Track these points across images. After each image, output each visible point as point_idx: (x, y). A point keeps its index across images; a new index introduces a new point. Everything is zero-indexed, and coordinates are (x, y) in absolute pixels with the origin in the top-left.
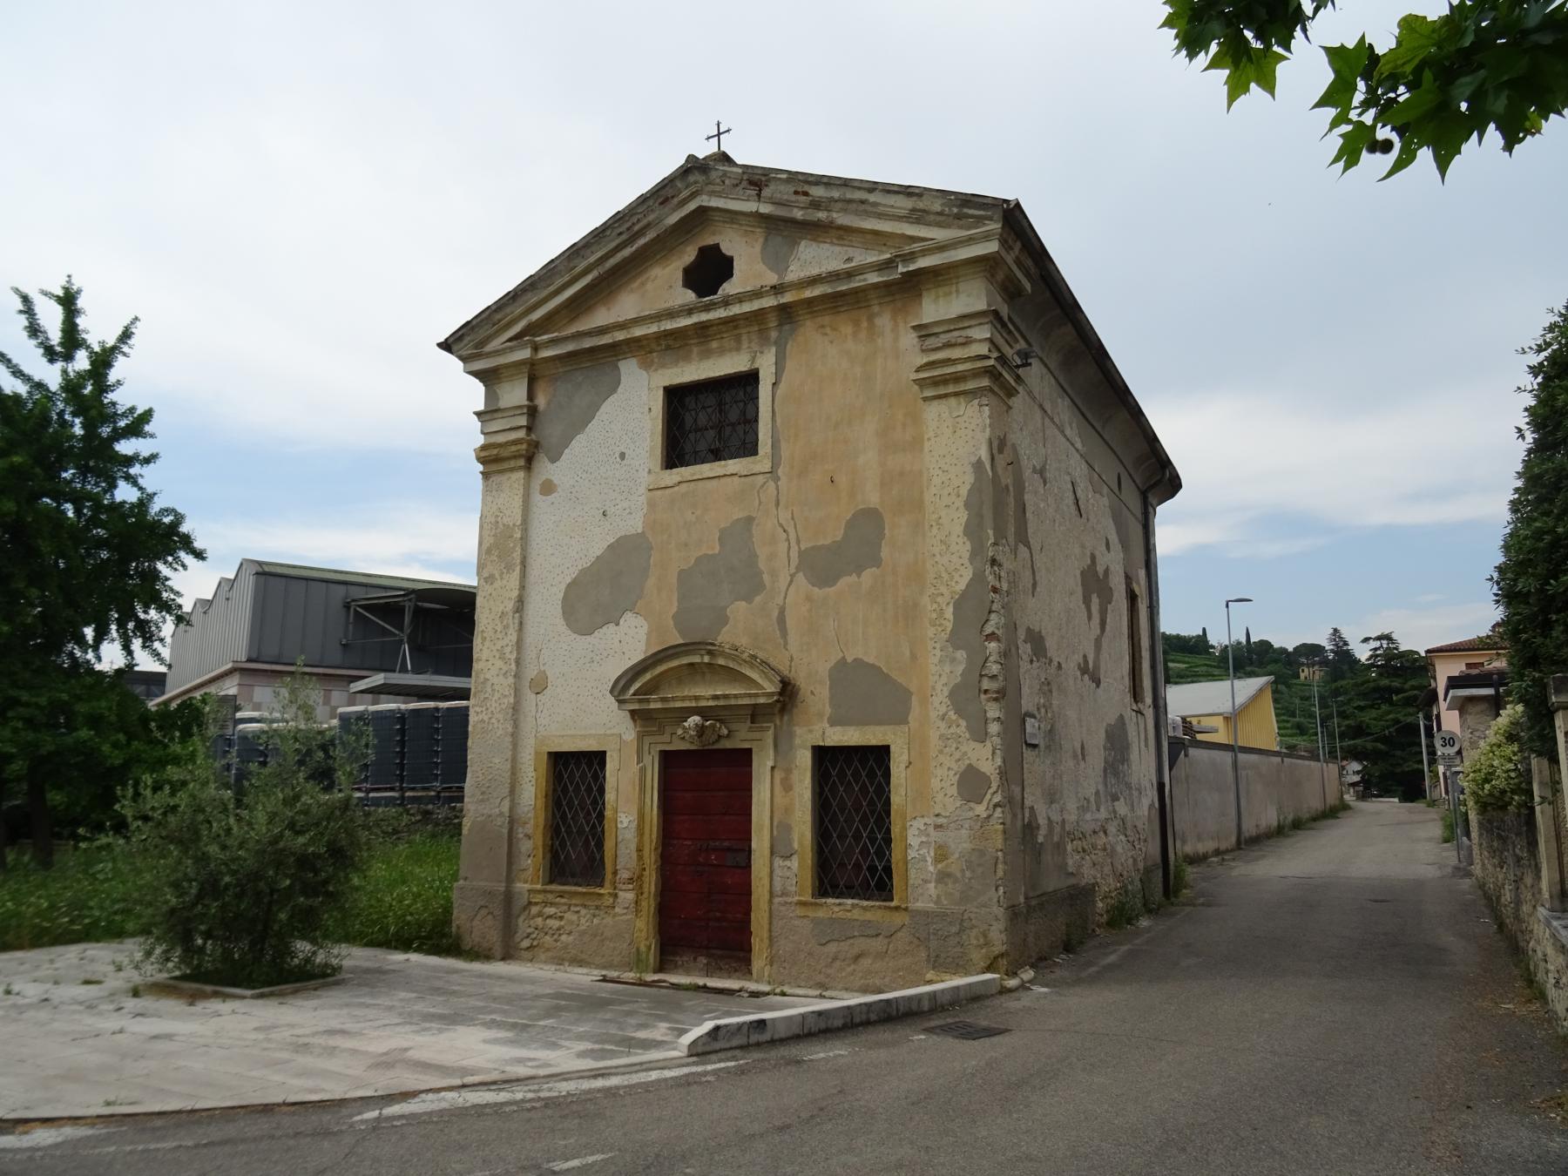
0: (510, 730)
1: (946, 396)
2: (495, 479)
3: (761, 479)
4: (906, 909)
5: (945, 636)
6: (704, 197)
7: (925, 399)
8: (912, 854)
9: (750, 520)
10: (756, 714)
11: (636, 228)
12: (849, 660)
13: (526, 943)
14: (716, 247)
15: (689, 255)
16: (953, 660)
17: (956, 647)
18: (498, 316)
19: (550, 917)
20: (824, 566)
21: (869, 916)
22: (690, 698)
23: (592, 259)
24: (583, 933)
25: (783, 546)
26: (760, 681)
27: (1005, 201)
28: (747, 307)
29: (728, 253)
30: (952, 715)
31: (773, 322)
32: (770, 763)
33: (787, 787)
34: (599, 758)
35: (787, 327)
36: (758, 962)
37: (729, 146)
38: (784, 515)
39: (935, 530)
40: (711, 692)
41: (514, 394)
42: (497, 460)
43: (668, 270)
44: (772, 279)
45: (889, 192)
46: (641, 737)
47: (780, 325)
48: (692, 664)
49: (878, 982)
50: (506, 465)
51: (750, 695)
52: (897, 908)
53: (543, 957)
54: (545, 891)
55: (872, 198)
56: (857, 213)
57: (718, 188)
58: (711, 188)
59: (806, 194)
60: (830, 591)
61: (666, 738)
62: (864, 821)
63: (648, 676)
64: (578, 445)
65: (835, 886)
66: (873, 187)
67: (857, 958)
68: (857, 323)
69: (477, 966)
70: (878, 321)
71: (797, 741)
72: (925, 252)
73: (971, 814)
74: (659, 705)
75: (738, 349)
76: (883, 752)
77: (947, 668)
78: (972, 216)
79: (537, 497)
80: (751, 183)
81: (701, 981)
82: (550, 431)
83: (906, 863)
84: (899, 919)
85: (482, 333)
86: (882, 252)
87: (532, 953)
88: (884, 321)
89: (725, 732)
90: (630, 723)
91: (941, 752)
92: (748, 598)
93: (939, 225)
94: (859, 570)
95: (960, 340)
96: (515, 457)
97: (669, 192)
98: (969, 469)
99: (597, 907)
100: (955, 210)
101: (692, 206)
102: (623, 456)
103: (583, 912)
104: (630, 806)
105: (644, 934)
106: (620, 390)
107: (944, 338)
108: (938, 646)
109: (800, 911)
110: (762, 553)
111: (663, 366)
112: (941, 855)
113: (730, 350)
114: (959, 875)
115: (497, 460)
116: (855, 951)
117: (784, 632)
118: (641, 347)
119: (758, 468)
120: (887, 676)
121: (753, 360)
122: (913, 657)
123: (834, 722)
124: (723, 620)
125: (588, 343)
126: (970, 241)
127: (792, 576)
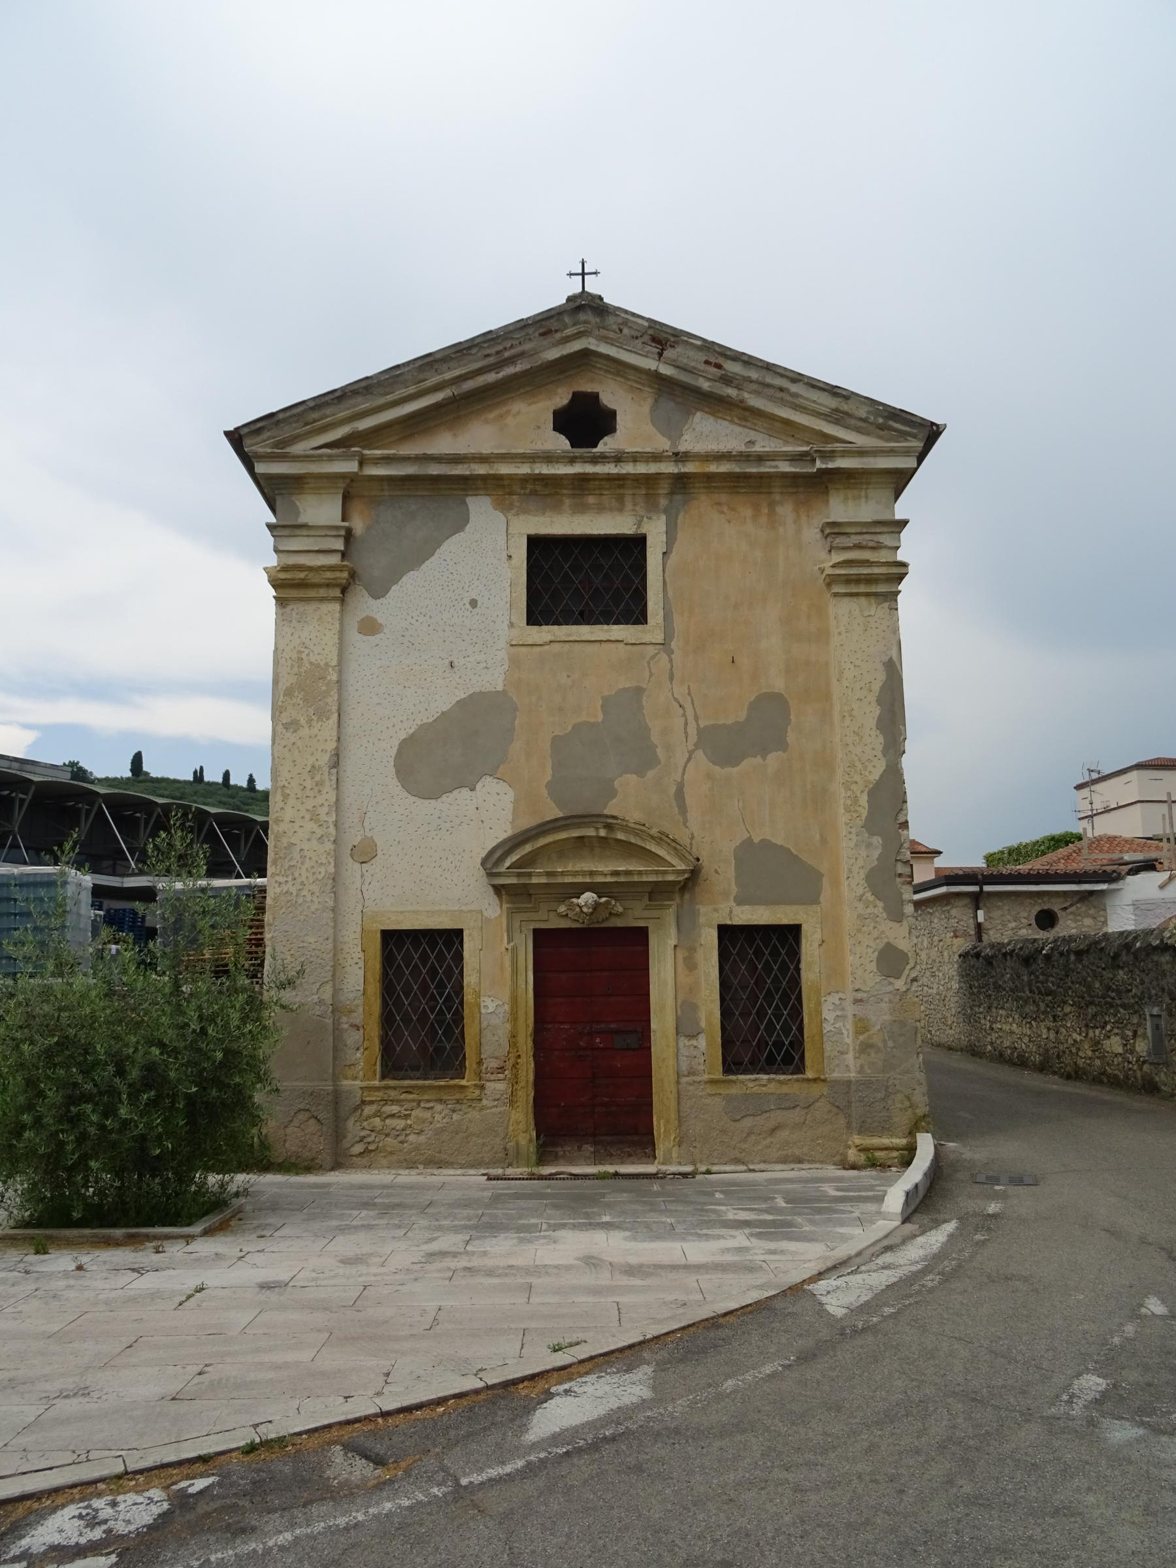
0: (331, 903)
1: (857, 595)
2: (295, 609)
3: (651, 650)
4: (824, 1081)
5: (861, 823)
6: (591, 340)
7: (836, 595)
8: (827, 1027)
9: (639, 691)
10: (658, 892)
11: (507, 354)
12: (756, 840)
13: (358, 1148)
14: (595, 397)
15: (561, 398)
16: (869, 845)
17: (872, 834)
18: (315, 415)
19: (393, 1116)
20: (724, 746)
21: (785, 1089)
22: (583, 873)
23: (448, 376)
24: (439, 1132)
25: (678, 722)
26: (668, 858)
27: (933, 424)
28: (641, 469)
29: (612, 406)
30: (869, 896)
31: (664, 488)
32: (673, 942)
33: (691, 965)
34: (454, 937)
35: (678, 497)
36: (664, 1142)
37: (593, 286)
38: (680, 691)
39: (847, 721)
40: (611, 868)
41: (322, 510)
42: (302, 585)
43: (533, 407)
44: (662, 444)
45: (814, 386)
46: (511, 913)
47: (672, 493)
48: (581, 838)
49: (797, 1152)
50: (312, 593)
51: (657, 872)
52: (815, 1080)
53: (384, 1162)
54: (387, 1088)
55: (794, 388)
56: (771, 398)
57: (612, 335)
58: (603, 332)
59: (719, 366)
60: (735, 770)
61: (542, 915)
62: (769, 996)
63: (528, 848)
64: (410, 584)
65: (738, 1064)
66: (797, 378)
67: (773, 1130)
68: (756, 508)
69: (311, 1179)
70: (780, 510)
71: (702, 920)
72: (845, 454)
73: (890, 988)
74: (544, 880)
75: (621, 510)
76: (794, 931)
77: (864, 853)
78: (896, 430)
79: (354, 636)
80: (654, 339)
81: (611, 1169)
82: (372, 562)
83: (822, 1035)
84: (816, 1090)
85: (286, 432)
86: (786, 443)
87: (369, 1157)
88: (786, 510)
89: (620, 909)
90: (494, 899)
91: (859, 931)
92: (640, 773)
93: (858, 430)
94: (764, 753)
95: (871, 544)
96: (328, 585)
97: (553, 324)
98: (881, 667)
99: (458, 1102)
100: (881, 420)
101: (576, 346)
102: (474, 603)
103: (438, 1107)
104: (497, 990)
105: (522, 1126)
106: (467, 528)
107: (856, 539)
108: (854, 830)
109: (710, 1089)
110: (655, 727)
111: (526, 512)
112: (862, 1026)
113: (611, 509)
114: (880, 1045)
115: (302, 585)
116: (771, 1124)
117: (683, 809)
118: (503, 486)
119: (647, 638)
120: (796, 856)
121: (639, 524)
122: (824, 840)
123: (740, 901)
124: (613, 793)
125: (434, 470)
126: (892, 452)
127: (691, 753)
